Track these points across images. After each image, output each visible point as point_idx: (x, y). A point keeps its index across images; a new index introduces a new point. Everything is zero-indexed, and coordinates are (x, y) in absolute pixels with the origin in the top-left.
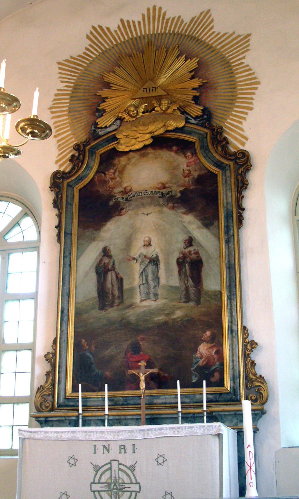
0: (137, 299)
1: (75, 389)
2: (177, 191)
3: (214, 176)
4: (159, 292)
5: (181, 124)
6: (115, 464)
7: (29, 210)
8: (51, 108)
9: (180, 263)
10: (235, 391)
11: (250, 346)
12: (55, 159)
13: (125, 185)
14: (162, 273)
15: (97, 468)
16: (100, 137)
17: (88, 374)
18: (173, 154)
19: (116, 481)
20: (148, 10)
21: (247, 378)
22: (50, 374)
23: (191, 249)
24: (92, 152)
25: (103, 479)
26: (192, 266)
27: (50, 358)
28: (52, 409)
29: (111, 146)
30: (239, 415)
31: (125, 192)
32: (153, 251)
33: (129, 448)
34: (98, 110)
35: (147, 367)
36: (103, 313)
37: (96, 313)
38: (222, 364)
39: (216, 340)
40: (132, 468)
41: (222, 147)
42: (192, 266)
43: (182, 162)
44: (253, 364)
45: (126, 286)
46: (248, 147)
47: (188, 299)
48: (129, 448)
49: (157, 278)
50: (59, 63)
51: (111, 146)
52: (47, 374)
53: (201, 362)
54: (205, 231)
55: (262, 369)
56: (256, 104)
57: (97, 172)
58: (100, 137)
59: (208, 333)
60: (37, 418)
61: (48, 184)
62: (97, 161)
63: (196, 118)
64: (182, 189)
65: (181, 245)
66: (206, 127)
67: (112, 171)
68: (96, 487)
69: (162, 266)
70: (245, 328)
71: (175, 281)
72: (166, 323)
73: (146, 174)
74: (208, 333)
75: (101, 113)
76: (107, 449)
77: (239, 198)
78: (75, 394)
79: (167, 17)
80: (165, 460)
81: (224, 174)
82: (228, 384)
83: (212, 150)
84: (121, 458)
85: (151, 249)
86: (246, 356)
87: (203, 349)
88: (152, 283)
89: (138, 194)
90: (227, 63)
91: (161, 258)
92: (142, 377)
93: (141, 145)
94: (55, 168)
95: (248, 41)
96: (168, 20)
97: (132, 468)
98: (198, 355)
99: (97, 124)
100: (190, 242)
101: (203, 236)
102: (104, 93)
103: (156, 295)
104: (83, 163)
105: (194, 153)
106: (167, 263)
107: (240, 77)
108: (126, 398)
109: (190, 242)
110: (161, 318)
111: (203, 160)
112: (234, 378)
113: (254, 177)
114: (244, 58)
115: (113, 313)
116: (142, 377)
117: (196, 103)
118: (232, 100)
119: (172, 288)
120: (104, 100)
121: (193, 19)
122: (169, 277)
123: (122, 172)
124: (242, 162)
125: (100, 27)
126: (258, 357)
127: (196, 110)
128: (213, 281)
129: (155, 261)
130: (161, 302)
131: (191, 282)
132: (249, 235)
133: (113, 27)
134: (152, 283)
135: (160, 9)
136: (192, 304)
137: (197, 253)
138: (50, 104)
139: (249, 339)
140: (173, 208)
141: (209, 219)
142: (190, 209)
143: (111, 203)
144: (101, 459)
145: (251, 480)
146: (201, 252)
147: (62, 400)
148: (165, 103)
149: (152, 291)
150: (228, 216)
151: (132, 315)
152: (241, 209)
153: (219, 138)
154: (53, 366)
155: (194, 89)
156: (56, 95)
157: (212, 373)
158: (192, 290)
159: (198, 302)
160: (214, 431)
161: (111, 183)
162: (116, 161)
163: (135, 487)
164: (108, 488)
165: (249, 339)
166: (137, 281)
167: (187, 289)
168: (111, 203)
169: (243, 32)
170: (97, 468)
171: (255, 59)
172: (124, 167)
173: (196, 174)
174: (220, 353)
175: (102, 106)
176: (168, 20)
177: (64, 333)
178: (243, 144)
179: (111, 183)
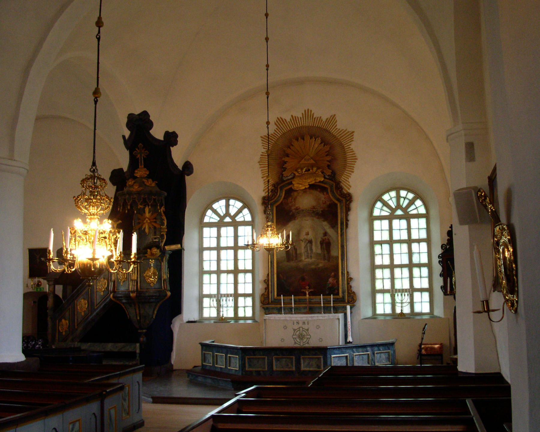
0: (303, 258)
1: (279, 295)
2: (320, 210)
3: (336, 205)
4: (313, 255)
5: (322, 179)
6: (301, 329)
7: (246, 205)
8: (259, 162)
9: (322, 243)
10: (343, 297)
11: (350, 279)
12: (263, 189)
13: (297, 206)
14: (314, 248)
15: (295, 330)
16: (284, 181)
17: (283, 289)
18: (318, 192)
19: (301, 335)
20: (305, 111)
21: (348, 292)
22: (267, 289)
23: (326, 237)
24: (281, 188)
25: (297, 334)
26: (326, 244)
27: (266, 282)
28: (268, 304)
29: (290, 187)
30: (346, 309)
31: (297, 209)
32: (310, 237)
33: (306, 323)
34: (283, 168)
35: (309, 289)
36: (288, 263)
37: (286, 263)
38: (338, 287)
39: (336, 277)
40: (308, 330)
41: (340, 191)
42: (326, 244)
43: (322, 197)
44: (351, 287)
45: (298, 252)
46: (351, 191)
47: (324, 259)
48: (306, 323)
49: (311, 249)
50: (261, 137)
51: (290, 187)
52: (266, 289)
53: (330, 285)
54: (332, 230)
55: (354, 289)
56: (355, 170)
57: (284, 198)
58: (284, 181)
59: (333, 274)
60: (263, 308)
61: (260, 201)
62: (284, 193)
63: (329, 176)
64: (321, 209)
65: (322, 235)
66: (332, 181)
67: (291, 198)
68: (295, 337)
69: (314, 244)
70: (348, 272)
71: (319, 251)
72: (315, 269)
73: (306, 201)
74: (333, 274)
75: (285, 169)
76: (298, 323)
77: (347, 215)
78: (279, 298)
79: (314, 117)
80: (319, 327)
81: (340, 204)
82: (341, 295)
83: (335, 193)
84: (304, 326)
85: (309, 236)
86: (348, 284)
87: (331, 280)
88: (309, 251)
89: (303, 210)
90: (343, 147)
91: (313, 240)
92: (307, 293)
93: (304, 188)
94: (263, 194)
95: (353, 135)
96: (315, 118)
97: (308, 330)
98: (329, 282)
99: (283, 175)
100: (325, 234)
101: (330, 231)
102: (286, 159)
103: (311, 257)
104: (277, 193)
105: (327, 193)
106: (316, 243)
107: (349, 155)
108: (299, 299)
109: (325, 234)
110: (313, 267)
111: (331, 196)
112: (343, 292)
113: (353, 205)
114: (350, 145)
115: (293, 264)
116: (307, 293)
117: (329, 169)
118: (345, 167)
119: (317, 255)
120: (285, 163)
121: (327, 119)
122: (317, 249)
123: (295, 199)
124: (348, 198)
125: (281, 118)
126: (353, 284)
127: (328, 172)
128: (336, 252)
129: (310, 242)
130: (313, 259)
131: (326, 252)
132: (351, 232)
133: (288, 120)
134: (309, 251)
135: (311, 111)
136: (326, 261)
137: (328, 239)
138: (259, 160)
139: (350, 277)
140: (318, 218)
141: (334, 225)
142: (326, 219)
143: (291, 214)
144: (296, 327)
145: (349, 334)
146: (330, 238)
147: (273, 299)
148: (315, 169)
149: (310, 255)
150: (342, 224)
151: (301, 265)
152: (347, 220)
153: (339, 187)
154: (268, 285)
155: (328, 161)
156: (261, 155)
157: (334, 290)
158: (326, 255)
159: (329, 261)
160: (337, 317)
161: (290, 205)
162: (292, 194)
163: (309, 337)
164: (299, 337)
165: (350, 277)
166: (303, 251)
167: (324, 254)
168: (291, 214)
169: (350, 130)
170: (295, 330)
171: (356, 146)
172: (296, 197)
173: (328, 203)
174: (338, 282)
175: (285, 166)
176: (315, 118)
177: (272, 271)
178: (349, 189)
179: (290, 205)
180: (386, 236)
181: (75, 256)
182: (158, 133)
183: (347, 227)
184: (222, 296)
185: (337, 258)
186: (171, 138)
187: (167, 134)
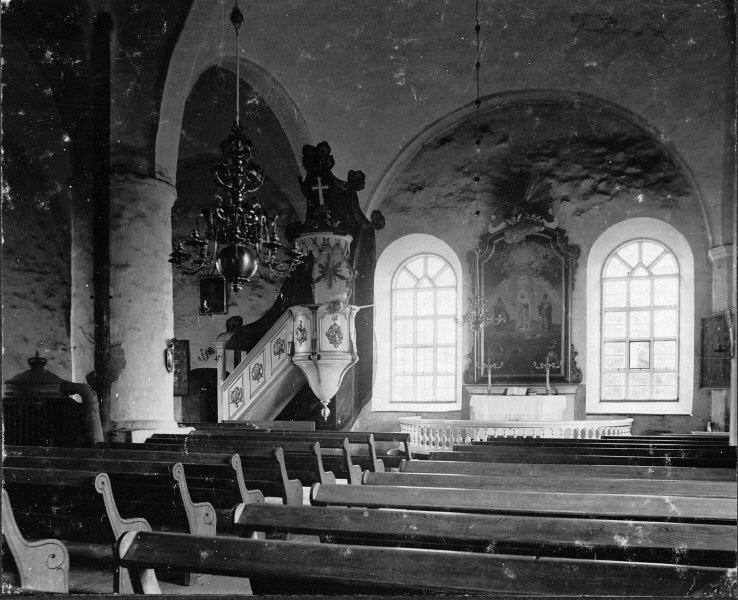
9: (540, 308)
26: (547, 311)
32: (526, 300)
42: (547, 311)
44: (575, 363)
69: (530, 308)
101: (551, 293)
122: (534, 315)
129: (526, 306)
131: (546, 319)
180: (659, 315)
181: (165, 347)
182: (340, 172)
183: (573, 288)
184: (438, 346)
185: (559, 326)
186: (357, 180)
187: (352, 174)
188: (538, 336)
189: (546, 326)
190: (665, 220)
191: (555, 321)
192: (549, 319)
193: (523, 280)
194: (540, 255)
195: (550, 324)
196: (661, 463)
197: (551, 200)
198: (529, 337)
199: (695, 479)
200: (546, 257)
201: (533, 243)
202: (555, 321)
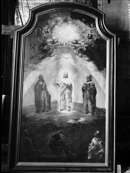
69: (73, 90)
122: (78, 97)
129: (69, 87)
131: (89, 103)
188: (82, 120)
189: (90, 110)
190: (82, 21)
191: (99, 105)
192: (94, 102)
193: (67, 60)
194: (86, 35)
195: (94, 108)
196: (36, 3)
197: (61, 57)
198: (71, 121)
199: (106, 72)
200: (91, 37)
201: (79, 22)
202: (99, 105)
